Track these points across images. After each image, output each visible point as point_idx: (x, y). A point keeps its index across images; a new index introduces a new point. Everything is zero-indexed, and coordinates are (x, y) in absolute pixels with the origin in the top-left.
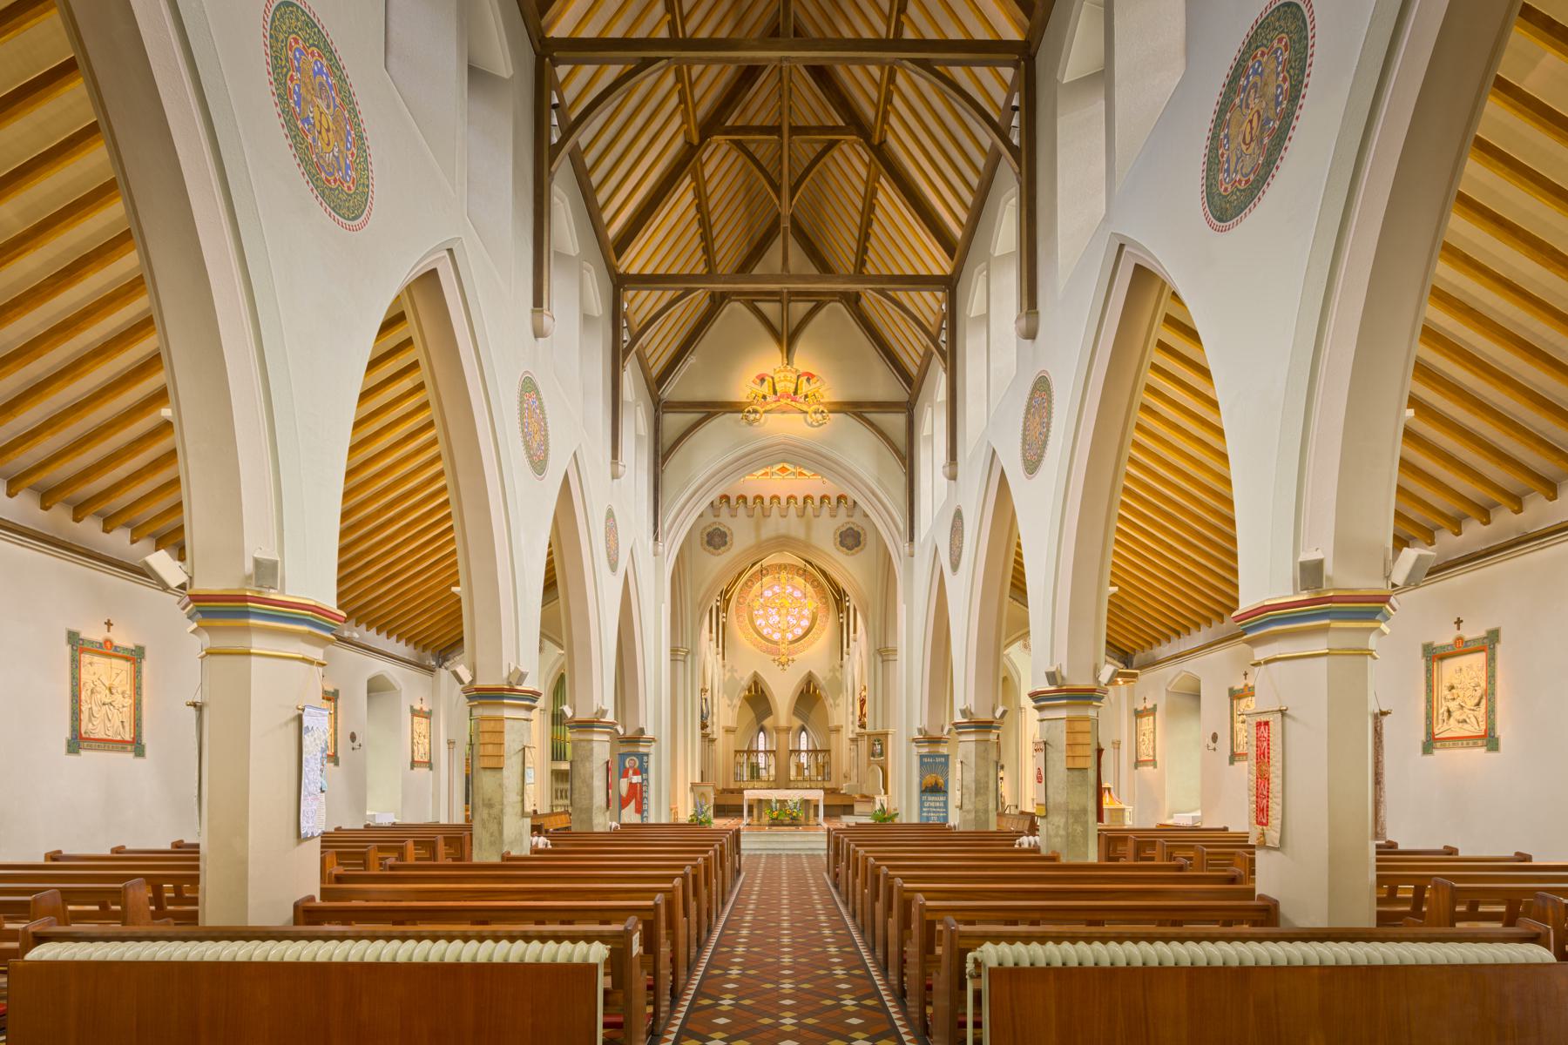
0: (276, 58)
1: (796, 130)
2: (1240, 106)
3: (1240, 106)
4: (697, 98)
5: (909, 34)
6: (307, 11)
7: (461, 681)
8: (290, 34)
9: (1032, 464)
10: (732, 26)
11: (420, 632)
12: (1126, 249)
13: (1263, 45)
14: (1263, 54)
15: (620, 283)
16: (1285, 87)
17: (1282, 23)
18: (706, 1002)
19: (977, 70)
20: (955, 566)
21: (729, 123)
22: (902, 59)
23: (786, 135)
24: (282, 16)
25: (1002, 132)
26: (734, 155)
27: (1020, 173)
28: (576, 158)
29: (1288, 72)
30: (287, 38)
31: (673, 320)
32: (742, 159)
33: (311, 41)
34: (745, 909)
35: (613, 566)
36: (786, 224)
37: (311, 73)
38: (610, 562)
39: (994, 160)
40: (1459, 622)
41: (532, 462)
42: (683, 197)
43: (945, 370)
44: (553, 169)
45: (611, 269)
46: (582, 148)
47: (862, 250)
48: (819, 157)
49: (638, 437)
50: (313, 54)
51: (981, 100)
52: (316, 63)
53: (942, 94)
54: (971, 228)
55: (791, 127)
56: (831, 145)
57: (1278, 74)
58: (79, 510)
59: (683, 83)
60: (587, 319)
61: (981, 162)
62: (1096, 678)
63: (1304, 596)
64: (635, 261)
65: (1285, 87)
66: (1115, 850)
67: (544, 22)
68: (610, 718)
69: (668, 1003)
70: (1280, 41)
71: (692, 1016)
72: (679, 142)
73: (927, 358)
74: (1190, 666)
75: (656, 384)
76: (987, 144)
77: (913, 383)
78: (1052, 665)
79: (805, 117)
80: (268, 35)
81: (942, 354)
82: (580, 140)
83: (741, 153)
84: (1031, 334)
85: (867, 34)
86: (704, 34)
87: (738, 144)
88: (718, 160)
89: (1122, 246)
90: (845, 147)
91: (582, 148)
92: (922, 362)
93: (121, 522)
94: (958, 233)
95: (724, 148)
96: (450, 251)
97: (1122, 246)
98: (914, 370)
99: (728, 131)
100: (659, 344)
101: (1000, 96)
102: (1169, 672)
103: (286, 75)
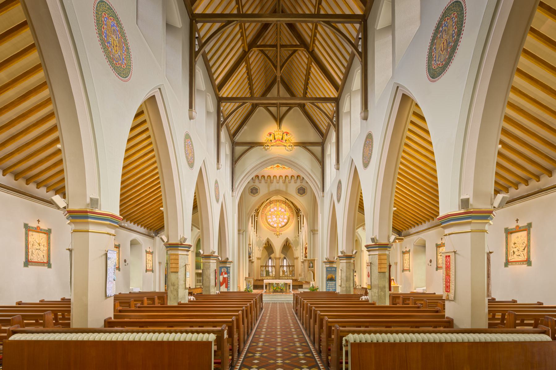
1: (282, 46)
4: (247, 35)
5: (322, 12)
9: (366, 164)
10: (259, 9)
11: (149, 224)
12: (399, 88)
15: (220, 100)
19: (346, 25)
20: (339, 200)
21: (258, 44)
22: (320, 21)
23: (279, 48)
25: (355, 47)
26: (260, 55)
27: (362, 61)
28: (204, 56)
32: (263, 56)
34: (264, 322)
35: (217, 200)
36: (279, 79)
38: (216, 199)
39: (352, 57)
40: (517, 220)
41: (189, 164)
42: (242, 70)
43: (335, 131)
44: (196, 60)
45: (217, 95)
46: (206, 53)
47: (306, 88)
48: (291, 55)
49: (226, 155)
51: (348, 35)
53: (334, 33)
54: (344, 81)
55: (280, 45)
56: (295, 51)
59: (242, 29)
60: (208, 113)
61: (348, 57)
62: (389, 240)
64: (225, 92)
66: (395, 301)
67: (193, 8)
68: (216, 254)
72: (241, 50)
73: (329, 127)
74: (422, 236)
75: (232, 136)
76: (350, 51)
77: (324, 136)
78: (373, 235)
79: (285, 42)
81: (334, 125)
82: (206, 50)
83: (263, 54)
84: (365, 118)
85: (307, 12)
86: (249, 12)
87: (262, 51)
88: (255, 57)
89: (398, 87)
90: (300, 52)
91: (206, 53)
92: (327, 128)
93: (43, 185)
94: (340, 82)
95: (257, 53)
97: (398, 87)
98: (324, 131)
99: (258, 47)
100: (234, 122)
101: (355, 34)
102: (415, 238)
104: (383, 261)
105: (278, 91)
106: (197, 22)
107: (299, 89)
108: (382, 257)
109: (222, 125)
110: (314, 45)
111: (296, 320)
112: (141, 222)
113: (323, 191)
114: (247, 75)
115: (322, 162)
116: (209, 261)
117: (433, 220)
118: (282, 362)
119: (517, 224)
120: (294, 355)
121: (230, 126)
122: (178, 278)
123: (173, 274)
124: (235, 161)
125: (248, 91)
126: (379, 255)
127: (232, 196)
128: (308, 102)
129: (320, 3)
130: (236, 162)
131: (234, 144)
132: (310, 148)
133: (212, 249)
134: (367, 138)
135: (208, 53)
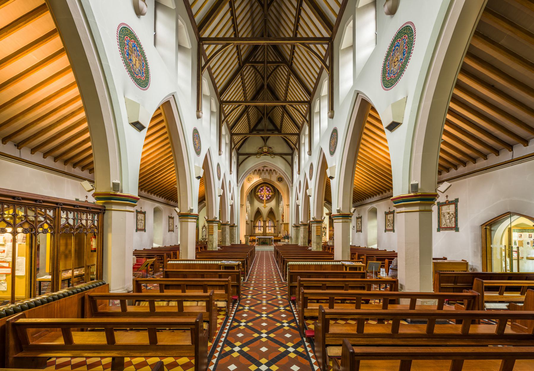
0: (121, 43)
1: (269, 62)
2: (393, 55)
3: (393, 55)
5: (299, 36)
6: (130, 29)
7: (177, 212)
8: (125, 36)
9: (332, 153)
11: (168, 196)
12: (359, 94)
13: (400, 38)
14: (400, 40)
15: (221, 103)
16: (406, 50)
17: (405, 31)
18: (241, 308)
19: (317, 45)
20: (311, 179)
22: (297, 43)
23: (266, 64)
24: (123, 30)
25: (324, 62)
26: (252, 68)
27: (329, 73)
28: (209, 69)
29: (407, 45)
30: (124, 37)
31: (240, 109)
33: (132, 38)
34: (255, 267)
35: (219, 179)
37: (131, 46)
38: (218, 177)
41: (196, 152)
44: (202, 73)
46: (211, 67)
47: (286, 94)
48: (275, 69)
49: (226, 144)
50: (132, 41)
51: (318, 53)
52: (133, 44)
53: (307, 52)
54: (315, 89)
55: (267, 62)
56: (278, 66)
57: (404, 46)
58: (75, 165)
60: (212, 113)
61: (318, 71)
62: (350, 211)
63: (412, 194)
65: (406, 50)
66: (353, 256)
67: (200, 33)
68: (218, 219)
69: (232, 305)
70: (405, 37)
71: (236, 313)
72: (237, 66)
73: (303, 122)
74: (374, 205)
75: (231, 128)
76: (320, 66)
77: (300, 128)
78: (338, 207)
79: (271, 59)
80: (118, 36)
81: (328, 68)
85: (287, 36)
86: (244, 36)
87: (254, 66)
89: (358, 94)
90: (282, 67)
91: (211, 67)
92: (307, 109)
93: (87, 168)
94: (312, 90)
95: (249, 67)
96: (173, 95)
97: (358, 94)
99: (252, 62)
100: (232, 119)
101: (324, 53)
102: (369, 207)
103: (124, 48)
104: (319, 230)
105: (265, 122)
106: (223, 105)
107: (281, 92)
108: (318, 227)
109: (203, 68)
110: (299, 16)
111: (277, 269)
112: (157, 192)
113: (292, 183)
114: (229, 7)
115: (291, 165)
116: (225, 227)
117: (389, 192)
118: (266, 302)
119: (447, 199)
120: (273, 289)
121: (191, 4)
122: (213, 238)
123: (211, 236)
124: (239, 165)
125: (232, 33)
126: (317, 226)
127: (237, 186)
128: (298, 43)
129: (300, 5)
130: (240, 165)
131: (238, 154)
132: (284, 156)
133: (190, 207)
134: (311, 165)
135: (192, 5)
